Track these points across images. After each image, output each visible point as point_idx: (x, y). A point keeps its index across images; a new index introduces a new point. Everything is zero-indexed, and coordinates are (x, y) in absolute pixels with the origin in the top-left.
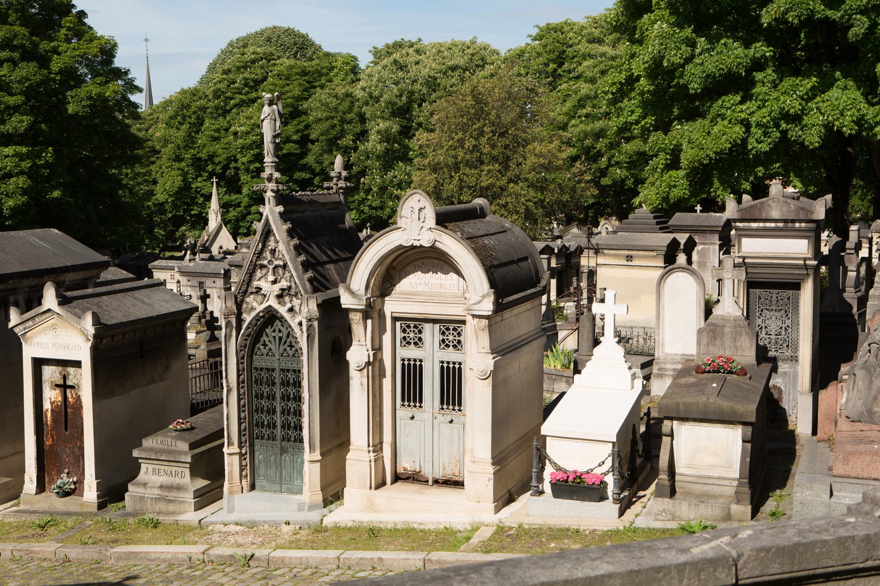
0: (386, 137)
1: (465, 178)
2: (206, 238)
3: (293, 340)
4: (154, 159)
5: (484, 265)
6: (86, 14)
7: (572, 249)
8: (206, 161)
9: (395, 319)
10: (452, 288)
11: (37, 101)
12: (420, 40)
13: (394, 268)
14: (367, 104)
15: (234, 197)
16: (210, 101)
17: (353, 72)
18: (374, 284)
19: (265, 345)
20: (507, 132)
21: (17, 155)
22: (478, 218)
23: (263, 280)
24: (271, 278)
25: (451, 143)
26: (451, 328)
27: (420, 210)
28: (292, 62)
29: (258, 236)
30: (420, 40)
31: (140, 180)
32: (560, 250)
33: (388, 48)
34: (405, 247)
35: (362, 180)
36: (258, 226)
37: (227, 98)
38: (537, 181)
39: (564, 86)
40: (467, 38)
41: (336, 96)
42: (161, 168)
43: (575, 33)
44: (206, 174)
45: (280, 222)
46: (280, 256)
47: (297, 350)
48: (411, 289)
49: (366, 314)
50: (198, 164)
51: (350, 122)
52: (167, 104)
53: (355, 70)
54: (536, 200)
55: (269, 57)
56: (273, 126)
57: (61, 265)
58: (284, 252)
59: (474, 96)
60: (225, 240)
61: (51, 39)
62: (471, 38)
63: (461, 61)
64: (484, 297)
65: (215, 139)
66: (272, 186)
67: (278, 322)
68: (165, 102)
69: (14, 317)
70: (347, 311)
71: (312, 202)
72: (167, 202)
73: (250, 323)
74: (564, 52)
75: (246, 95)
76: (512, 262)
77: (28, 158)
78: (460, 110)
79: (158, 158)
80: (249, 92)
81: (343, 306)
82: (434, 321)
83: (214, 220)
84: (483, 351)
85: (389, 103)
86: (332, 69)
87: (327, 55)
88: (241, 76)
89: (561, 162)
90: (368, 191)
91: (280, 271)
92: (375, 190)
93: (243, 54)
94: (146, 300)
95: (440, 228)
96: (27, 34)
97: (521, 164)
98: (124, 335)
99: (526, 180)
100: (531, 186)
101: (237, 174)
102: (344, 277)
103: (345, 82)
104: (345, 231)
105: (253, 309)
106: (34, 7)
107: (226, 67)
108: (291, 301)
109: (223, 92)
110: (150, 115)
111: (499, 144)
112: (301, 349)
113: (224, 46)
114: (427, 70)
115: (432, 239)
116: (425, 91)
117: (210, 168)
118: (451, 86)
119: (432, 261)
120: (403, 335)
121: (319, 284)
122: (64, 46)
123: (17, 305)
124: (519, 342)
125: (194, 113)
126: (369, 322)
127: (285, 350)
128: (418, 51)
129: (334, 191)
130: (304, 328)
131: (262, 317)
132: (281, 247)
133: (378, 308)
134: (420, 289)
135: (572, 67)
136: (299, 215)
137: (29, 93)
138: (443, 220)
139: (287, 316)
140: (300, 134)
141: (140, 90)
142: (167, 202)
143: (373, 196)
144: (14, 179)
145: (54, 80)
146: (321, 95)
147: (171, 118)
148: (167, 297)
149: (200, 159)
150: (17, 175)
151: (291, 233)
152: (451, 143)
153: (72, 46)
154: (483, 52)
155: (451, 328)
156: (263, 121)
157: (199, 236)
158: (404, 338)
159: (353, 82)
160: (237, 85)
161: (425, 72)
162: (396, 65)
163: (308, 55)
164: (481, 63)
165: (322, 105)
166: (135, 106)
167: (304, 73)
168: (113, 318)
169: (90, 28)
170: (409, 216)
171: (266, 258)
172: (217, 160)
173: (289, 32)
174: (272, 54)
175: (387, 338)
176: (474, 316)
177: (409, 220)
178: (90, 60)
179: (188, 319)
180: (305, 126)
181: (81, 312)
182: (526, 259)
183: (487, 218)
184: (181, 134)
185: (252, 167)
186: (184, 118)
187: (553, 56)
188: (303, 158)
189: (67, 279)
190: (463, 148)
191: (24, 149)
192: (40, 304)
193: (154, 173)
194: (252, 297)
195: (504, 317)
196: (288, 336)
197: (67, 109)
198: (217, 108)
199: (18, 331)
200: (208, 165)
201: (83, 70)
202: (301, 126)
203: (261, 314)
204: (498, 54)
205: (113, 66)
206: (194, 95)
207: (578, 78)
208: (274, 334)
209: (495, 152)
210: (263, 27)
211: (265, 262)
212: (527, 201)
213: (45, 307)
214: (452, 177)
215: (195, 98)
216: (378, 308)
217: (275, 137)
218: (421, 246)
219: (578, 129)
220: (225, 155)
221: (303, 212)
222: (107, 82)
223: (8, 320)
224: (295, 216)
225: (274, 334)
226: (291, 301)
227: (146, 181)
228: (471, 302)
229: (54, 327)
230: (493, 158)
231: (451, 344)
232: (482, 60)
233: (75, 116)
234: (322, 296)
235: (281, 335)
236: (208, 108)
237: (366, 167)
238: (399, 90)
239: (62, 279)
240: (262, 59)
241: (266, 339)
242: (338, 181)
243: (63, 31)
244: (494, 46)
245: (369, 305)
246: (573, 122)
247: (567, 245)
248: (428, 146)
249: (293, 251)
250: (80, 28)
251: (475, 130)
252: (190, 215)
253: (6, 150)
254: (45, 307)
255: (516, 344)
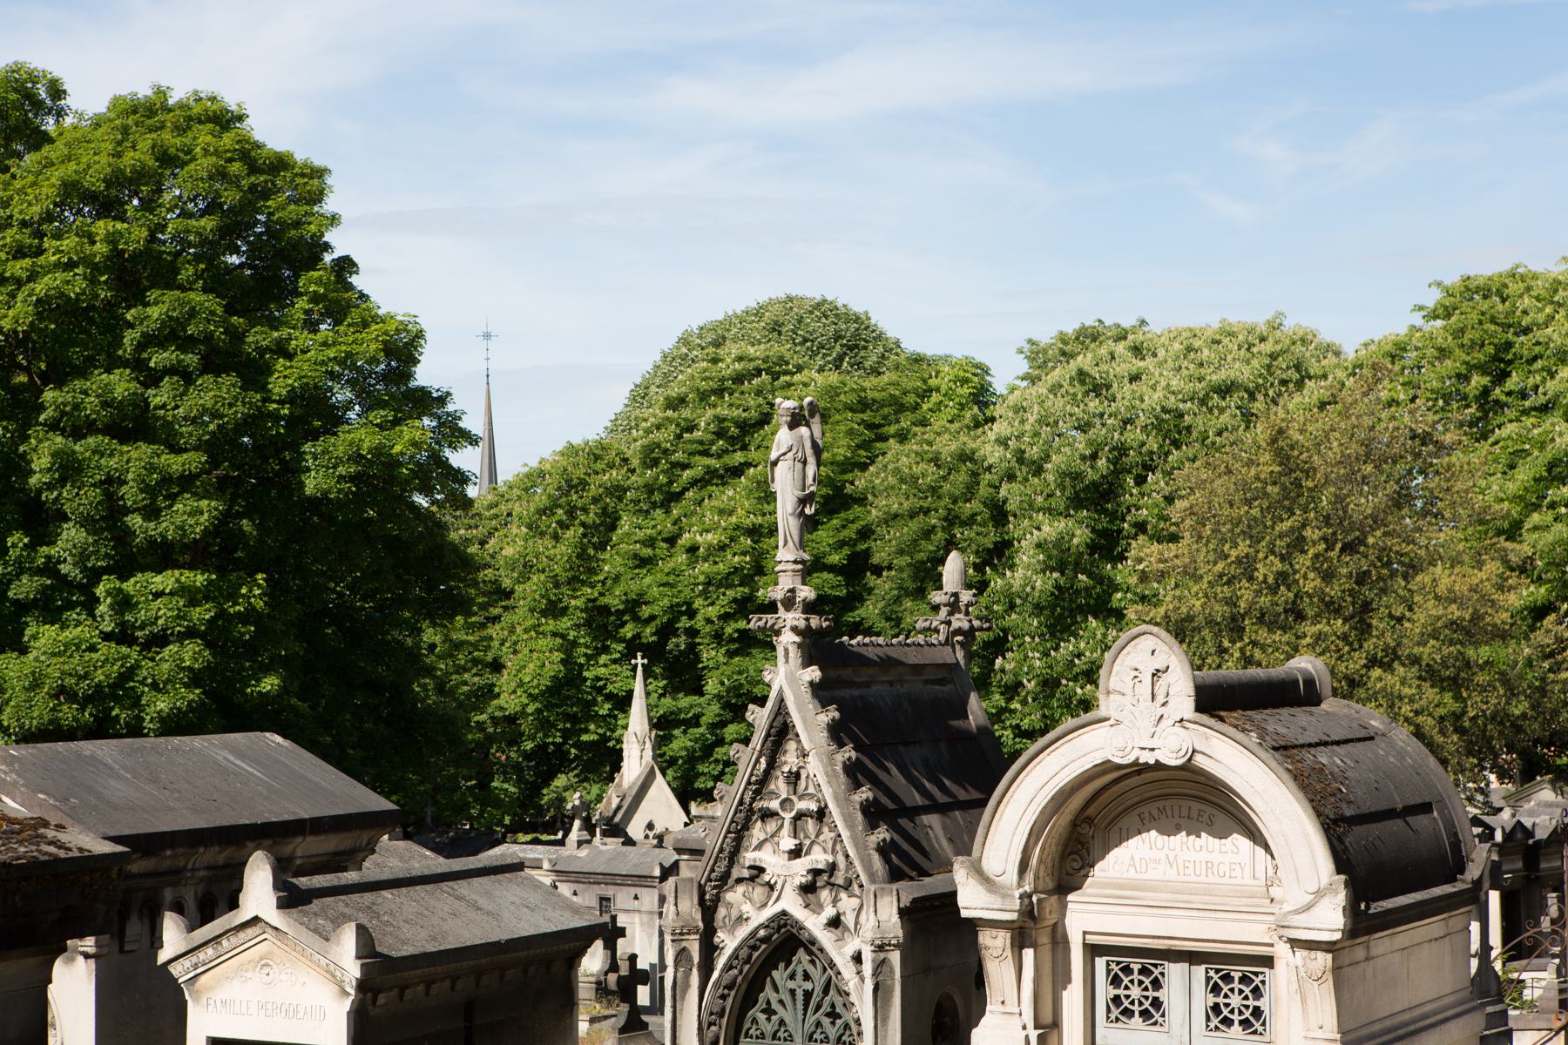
0: (1059, 558)
1: (1258, 654)
2: (615, 802)
3: (839, 1001)
4: (495, 611)
5: (1319, 814)
6: (354, 264)
7: (1542, 834)
8: (620, 613)
9: (1093, 951)
10: (1238, 872)
11: (234, 467)
12: (1143, 322)
13: (1090, 821)
14: (1011, 477)
15: (685, 701)
16: (633, 471)
17: (977, 403)
18: (1040, 861)
19: (769, 1011)
20: (1362, 542)
21: (182, 590)
22: (1300, 705)
23: (768, 847)
24: (788, 843)
25: (1220, 567)
26: (1237, 975)
27: (1156, 674)
28: (834, 378)
29: (757, 740)
30: (1143, 322)
31: (462, 658)
32: (1508, 836)
33: (1065, 342)
34: (1120, 767)
35: (999, 661)
36: (759, 716)
37: (674, 465)
38: (1444, 664)
39: (1510, 429)
40: (1258, 317)
41: (936, 460)
42: (512, 631)
43: (1538, 299)
44: (620, 647)
45: (811, 705)
46: (811, 790)
47: (847, 1026)
48: (1132, 874)
49: (1022, 934)
50: (601, 622)
51: (970, 521)
52: (533, 478)
53: (981, 396)
54: (1441, 711)
55: (776, 370)
56: (798, 475)
57: (286, 817)
58: (822, 779)
59: (1279, 452)
60: (661, 808)
61: (274, 324)
62: (1269, 315)
63: (1243, 372)
64: (1319, 894)
65: (644, 562)
66: (794, 618)
67: (801, 954)
68: (529, 476)
69: (173, 936)
70: (973, 925)
71: (889, 663)
72: (523, 714)
73: (735, 955)
74: (1509, 345)
75: (719, 456)
76: (1390, 814)
77: (207, 598)
78: (1245, 486)
79: (506, 608)
80: (726, 451)
81: (964, 914)
82: (1192, 958)
83: (636, 758)
84: (1320, 1034)
85: (1064, 474)
86: (926, 393)
87: (918, 360)
88: (710, 413)
89: (1505, 616)
90: (1012, 690)
91: (811, 825)
92: (1030, 686)
93: (715, 361)
94: (482, 902)
95: (1204, 718)
96: (219, 311)
97: (1400, 620)
98: (428, 985)
99: (1415, 660)
100: (1430, 674)
101: (692, 647)
102: (964, 844)
103: (957, 425)
104: (966, 736)
105: (741, 919)
106: (237, 251)
107: (674, 391)
108: (835, 901)
109: (666, 451)
110: (491, 507)
111: (1344, 571)
112: (858, 1022)
113: (668, 342)
114: (1159, 394)
115: (1187, 745)
116: (1153, 444)
117: (628, 631)
118: (1219, 434)
119: (1185, 803)
120: (1113, 992)
121: (903, 861)
122: (301, 339)
123: (179, 908)
124: (1414, 1021)
125: (595, 500)
126: (1028, 954)
127: (818, 1024)
128: (1137, 350)
129: (942, 638)
130: (867, 968)
131: (763, 940)
132: (815, 767)
133: (1051, 919)
134: (1154, 874)
135: (1531, 382)
136: (856, 693)
137: (218, 447)
138: (1214, 701)
139: (825, 938)
140: (846, 551)
141: (473, 440)
142: (523, 714)
143: (1024, 703)
144: (173, 648)
145: (276, 417)
146: (897, 457)
147: (542, 512)
148: (534, 898)
149: (605, 610)
150: (181, 638)
151: (837, 733)
152: (1220, 567)
153: (319, 337)
154: (1299, 349)
155: (1237, 975)
156: (775, 463)
157: (599, 799)
158: (1116, 1000)
159: (977, 425)
160: (697, 434)
161: (1154, 399)
162: (1083, 382)
163: (867, 364)
164: (1295, 376)
165: (902, 481)
166: (461, 478)
167: (863, 405)
168: (404, 943)
169: (363, 297)
170: (1128, 691)
171: (774, 795)
172: (645, 611)
173: (823, 309)
174: (782, 361)
175: (1072, 999)
176: (1295, 943)
177: (1127, 700)
178: (359, 370)
179: (582, 952)
180: (859, 532)
181: (329, 926)
182: (1425, 808)
183: (1324, 706)
184: (563, 550)
185: (728, 630)
186: (571, 512)
187: (1479, 357)
188: (854, 609)
189: (299, 853)
190: (1251, 579)
191: (200, 578)
192: (234, 904)
193: (496, 644)
194: (741, 889)
195: (1374, 952)
196: (826, 991)
197: (302, 485)
198: (649, 489)
199: (179, 971)
200: (623, 624)
201: (342, 394)
202: (850, 532)
203: (762, 933)
204: (1337, 354)
205: (412, 384)
206: (597, 458)
207: (1544, 409)
208: (791, 985)
209: (1333, 591)
210: (763, 299)
211: (774, 805)
212: (1417, 713)
213: (244, 914)
214: (1225, 651)
215: (599, 466)
216: (1051, 919)
217: (803, 501)
218: (1159, 766)
219: (1549, 537)
220: (666, 602)
221: (868, 685)
222: (397, 422)
223: (156, 942)
224: (846, 693)
225: (791, 985)
226: (835, 901)
227: (476, 662)
228: (1287, 908)
229: (264, 963)
230: (1327, 605)
231: (1236, 1017)
232: (1298, 367)
233: (319, 503)
234: (910, 891)
235: (808, 985)
236: (629, 489)
237: (1005, 631)
238: (1090, 443)
239: (287, 850)
240: (758, 372)
241: (773, 997)
242: (951, 613)
243: (302, 304)
244: (1327, 335)
245: (1029, 913)
246: (1536, 518)
247: (1528, 822)
248: (1162, 575)
249: (842, 777)
250: (341, 299)
251: (1281, 536)
252: (579, 745)
253: (159, 578)
254: (244, 914)
255: (1406, 1024)
